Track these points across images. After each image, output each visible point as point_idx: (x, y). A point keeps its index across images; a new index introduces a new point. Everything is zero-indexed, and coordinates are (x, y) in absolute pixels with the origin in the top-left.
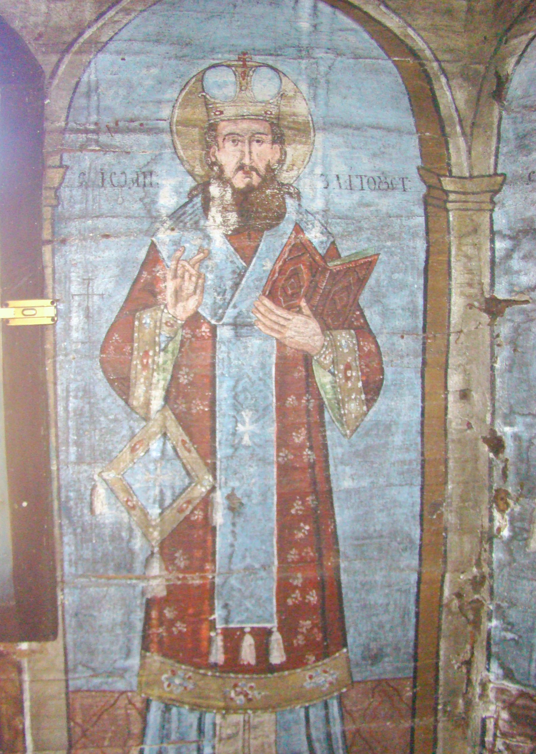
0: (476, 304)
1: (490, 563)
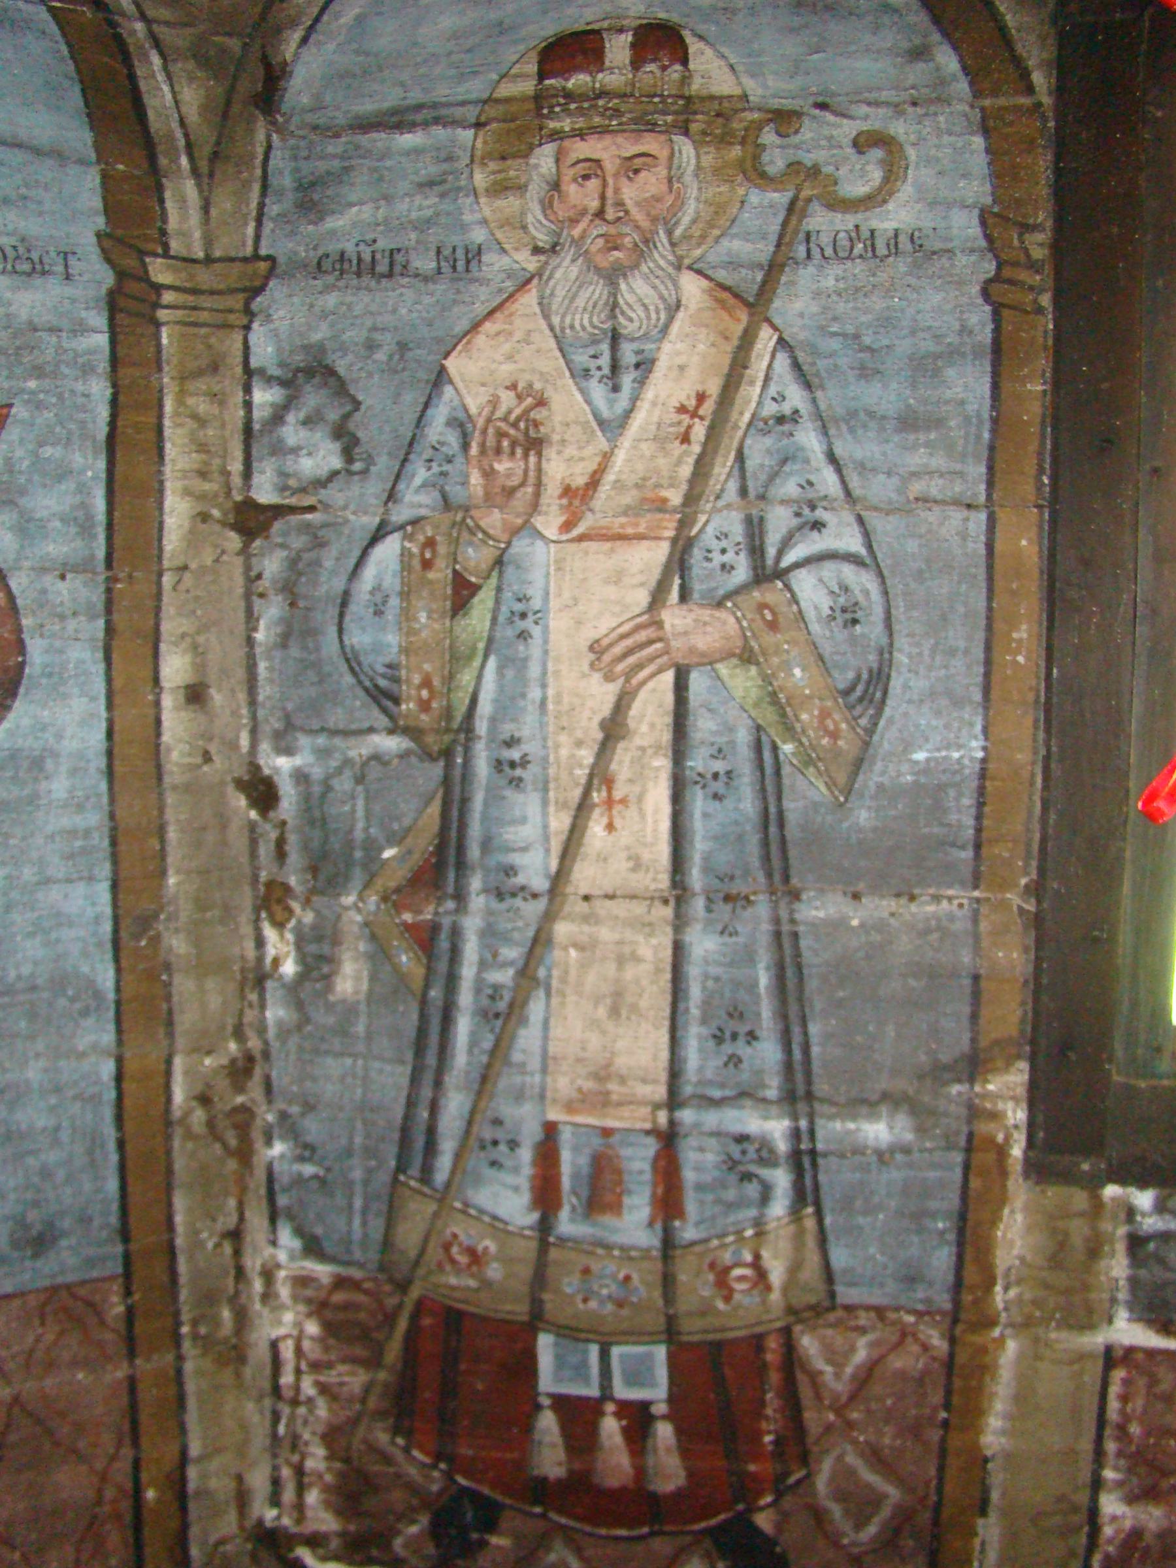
0: (216, 513)
1: (262, 1030)
